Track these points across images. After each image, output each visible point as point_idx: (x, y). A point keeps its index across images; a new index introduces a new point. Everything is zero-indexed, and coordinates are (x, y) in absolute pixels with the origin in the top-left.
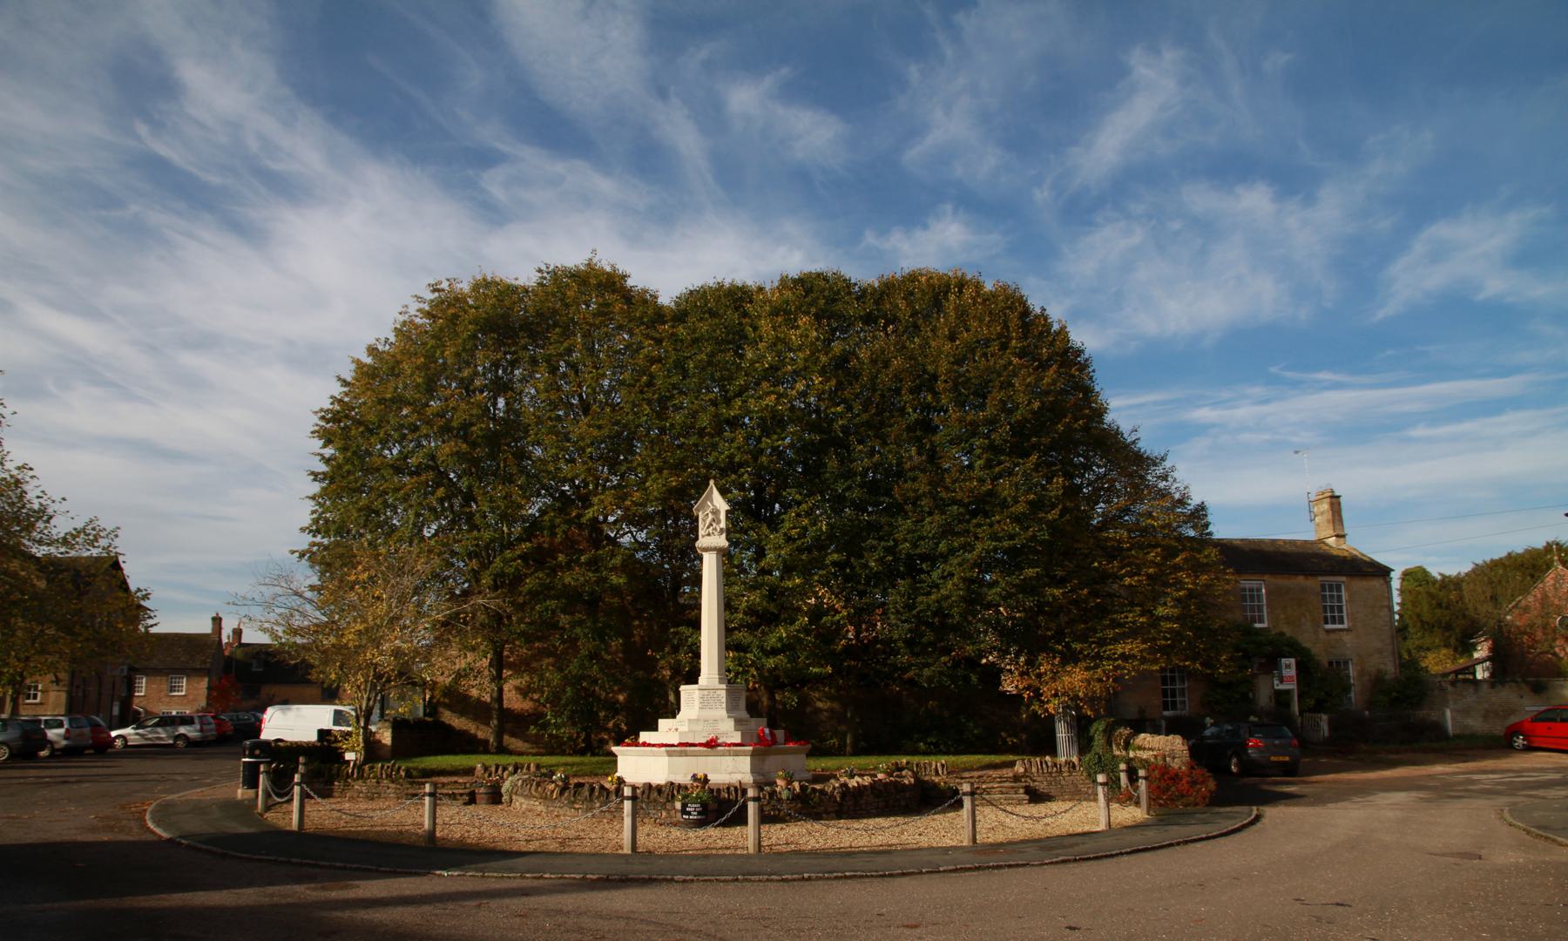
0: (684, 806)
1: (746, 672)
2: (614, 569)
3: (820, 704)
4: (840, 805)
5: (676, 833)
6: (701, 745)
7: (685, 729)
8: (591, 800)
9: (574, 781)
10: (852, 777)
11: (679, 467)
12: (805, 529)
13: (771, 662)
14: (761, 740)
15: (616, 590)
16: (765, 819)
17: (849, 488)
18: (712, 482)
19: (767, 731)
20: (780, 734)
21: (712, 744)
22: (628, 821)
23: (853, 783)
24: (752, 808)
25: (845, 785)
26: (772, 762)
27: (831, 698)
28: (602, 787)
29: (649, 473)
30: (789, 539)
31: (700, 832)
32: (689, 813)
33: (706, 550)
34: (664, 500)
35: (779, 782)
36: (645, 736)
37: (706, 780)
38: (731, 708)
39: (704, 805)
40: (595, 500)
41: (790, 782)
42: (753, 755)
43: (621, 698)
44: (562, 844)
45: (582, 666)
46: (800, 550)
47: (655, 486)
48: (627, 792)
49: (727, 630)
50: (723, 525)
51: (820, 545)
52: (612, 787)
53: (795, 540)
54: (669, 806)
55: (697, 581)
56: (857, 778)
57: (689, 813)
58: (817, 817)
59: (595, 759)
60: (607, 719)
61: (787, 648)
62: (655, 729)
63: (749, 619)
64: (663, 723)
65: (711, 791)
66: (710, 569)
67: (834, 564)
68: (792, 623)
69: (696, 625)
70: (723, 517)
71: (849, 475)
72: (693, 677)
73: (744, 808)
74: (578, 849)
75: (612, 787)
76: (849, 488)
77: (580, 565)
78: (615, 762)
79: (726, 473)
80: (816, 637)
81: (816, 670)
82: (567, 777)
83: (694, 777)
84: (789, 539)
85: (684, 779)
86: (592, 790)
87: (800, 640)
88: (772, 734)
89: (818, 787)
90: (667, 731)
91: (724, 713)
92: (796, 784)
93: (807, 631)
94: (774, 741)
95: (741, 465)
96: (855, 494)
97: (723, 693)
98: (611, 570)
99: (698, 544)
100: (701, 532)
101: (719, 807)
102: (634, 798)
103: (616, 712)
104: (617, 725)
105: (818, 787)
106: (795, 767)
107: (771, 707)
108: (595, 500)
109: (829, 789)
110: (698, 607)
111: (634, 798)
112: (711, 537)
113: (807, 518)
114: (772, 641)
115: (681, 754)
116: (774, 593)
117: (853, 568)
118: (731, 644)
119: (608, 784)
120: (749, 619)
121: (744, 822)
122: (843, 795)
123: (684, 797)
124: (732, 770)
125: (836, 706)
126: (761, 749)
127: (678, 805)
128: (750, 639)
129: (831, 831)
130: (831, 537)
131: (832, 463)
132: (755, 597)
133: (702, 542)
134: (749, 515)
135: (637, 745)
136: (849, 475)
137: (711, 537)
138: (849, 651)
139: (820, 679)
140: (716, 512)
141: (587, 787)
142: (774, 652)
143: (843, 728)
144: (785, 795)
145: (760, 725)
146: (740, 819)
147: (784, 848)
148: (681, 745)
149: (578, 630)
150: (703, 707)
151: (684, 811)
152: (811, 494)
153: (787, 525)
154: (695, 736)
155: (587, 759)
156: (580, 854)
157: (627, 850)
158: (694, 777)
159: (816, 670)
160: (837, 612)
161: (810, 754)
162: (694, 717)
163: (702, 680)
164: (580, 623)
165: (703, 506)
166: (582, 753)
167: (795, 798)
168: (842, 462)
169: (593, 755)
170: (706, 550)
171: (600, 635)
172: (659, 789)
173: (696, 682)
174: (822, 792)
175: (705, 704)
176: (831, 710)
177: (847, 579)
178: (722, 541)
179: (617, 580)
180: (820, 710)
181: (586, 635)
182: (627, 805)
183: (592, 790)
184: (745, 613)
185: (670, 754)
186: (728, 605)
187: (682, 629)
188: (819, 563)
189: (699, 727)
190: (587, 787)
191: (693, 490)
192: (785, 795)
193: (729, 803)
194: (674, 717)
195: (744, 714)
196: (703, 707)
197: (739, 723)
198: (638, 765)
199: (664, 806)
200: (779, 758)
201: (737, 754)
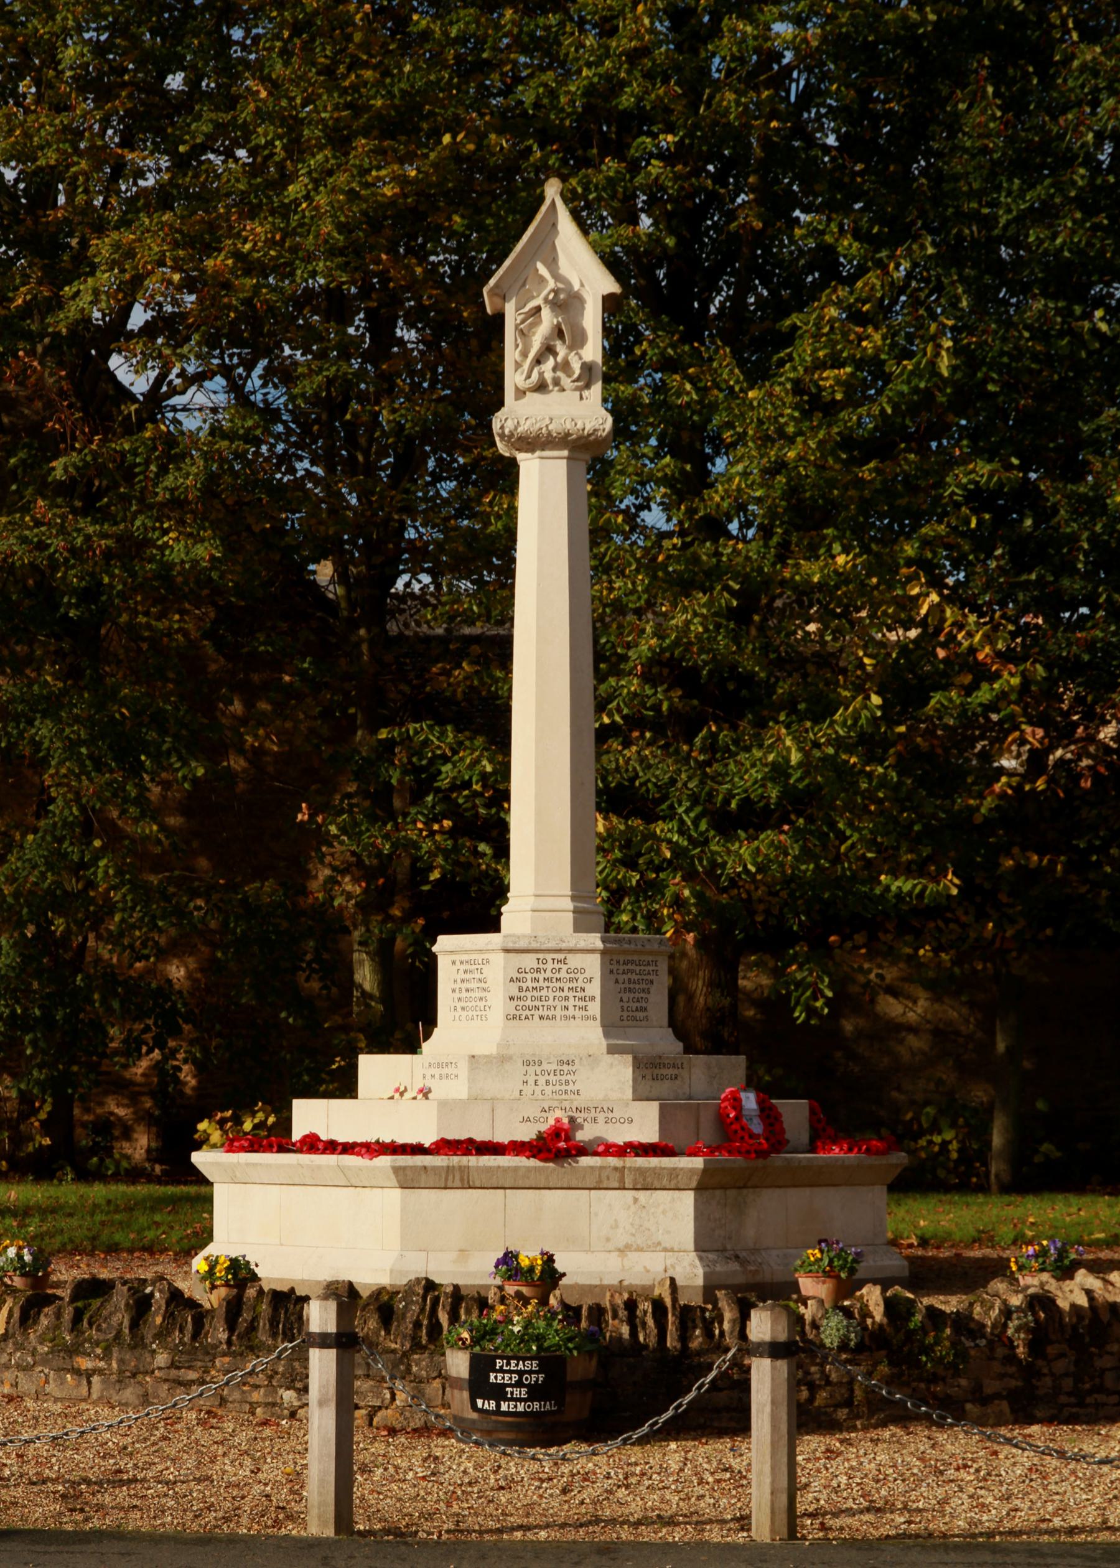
0: (481, 1366)
1: (650, 889)
2: (177, 503)
3: (892, 1008)
4: (1028, 1371)
5: (461, 1460)
6: (517, 1148)
7: (457, 1089)
8: (138, 1343)
9: (66, 1274)
10: (1065, 1272)
11: (402, 127)
12: (874, 366)
13: (742, 855)
14: (729, 1133)
15: (169, 588)
16: (806, 1417)
17: (1045, 214)
18: (552, 189)
19: (750, 1101)
20: (794, 1113)
21: (556, 1146)
22: (321, 1422)
23: (1072, 1293)
24: (765, 1380)
25: (1042, 1302)
26: (772, 1212)
27: (939, 987)
28: (176, 1297)
29: (297, 149)
30: (814, 405)
31: (544, 1459)
32: (498, 1393)
33: (532, 443)
34: (350, 254)
35: (808, 1285)
36: (309, 1115)
37: (548, 1275)
38: (619, 1020)
39: (552, 1364)
40: (102, 248)
41: (846, 1286)
42: (706, 1186)
43: (177, 972)
44: (71, 1498)
45: (56, 860)
46: (857, 448)
47: (319, 197)
48: (320, 1317)
49: (605, 730)
50: (593, 350)
51: (922, 419)
52: (212, 1299)
53: (830, 409)
54: (420, 1365)
55: (496, 553)
56: (1083, 1278)
57: (498, 1393)
58: (950, 1410)
59: (98, 1191)
60: (132, 1049)
61: (800, 803)
62: (345, 1085)
63: (665, 698)
64: (375, 1070)
65: (572, 1313)
66: (543, 508)
67: (977, 497)
68: (822, 710)
69: (489, 720)
70: (592, 319)
71: (1038, 158)
72: (477, 904)
73: (737, 1385)
74: (135, 1522)
75: (212, 1299)
76: (1045, 214)
77: (46, 488)
78: (209, 1200)
79: (590, 139)
80: (902, 767)
81: (903, 885)
82: (42, 1260)
83: (508, 1262)
84: (814, 405)
85: (477, 1270)
86: (141, 1306)
87: (844, 775)
88: (768, 1114)
89: (950, 1304)
90: (390, 1094)
91: (592, 1035)
92: (873, 1297)
93: (870, 744)
94: (776, 1139)
95: (638, 121)
96: (1066, 235)
97: (593, 965)
98: (163, 510)
99: (505, 421)
100: (513, 379)
101: (611, 1375)
102: (344, 1341)
103: (169, 1028)
104: (164, 1074)
105: (950, 1304)
106: (852, 1225)
107: (751, 1003)
108: (102, 248)
109: (987, 1315)
110: (499, 651)
111: (344, 1341)
112: (550, 400)
113: (873, 327)
114: (746, 776)
115: (447, 1181)
116: (752, 605)
117: (1045, 514)
118: (614, 798)
119: (193, 1277)
120: (665, 698)
121: (735, 1422)
122: (1038, 1338)
123: (482, 1335)
124: (633, 1240)
125: (952, 1012)
126: (735, 1165)
127: (458, 1363)
128: (664, 770)
129: (1014, 1463)
130: (966, 393)
131: (980, 115)
132: (689, 617)
133: (518, 413)
134: (657, 298)
135: (285, 1147)
136: (1038, 158)
137: (550, 400)
138: (1021, 816)
139: (913, 918)
140: (567, 303)
141: (120, 1298)
142: (750, 818)
143: (980, 1094)
144: (832, 1331)
145: (720, 1079)
146: (726, 1416)
147: (863, 1525)
148: (444, 1146)
149: (43, 730)
150: (522, 1013)
151: (479, 1385)
152: (898, 234)
153: (805, 350)
154: (491, 1118)
155: (68, 1191)
156: (155, 1539)
157: (318, 1523)
158: (508, 1262)
159: (903, 885)
160: (983, 674)
161: (904, 1185)
162: (489, 1047)
163: (515, 915)
164: (51, 705)
165: (522, 280)
166: (41, 1168)
167: (869, 1343)
168: (1015, 105)
169: (85, 1176)
170: (532, 443)
171: (122, 748)
172: (384, 1304)
173: (492, 925)
174: (963, 1323)
175: (525, 1004)
176: (941, 1033)
177: (1023, 555)
178: (590, 413)
179: (186, 549)
180: (897, 1028)
181: (72, 746)
182: (322, 1365)
183: (141, 1306)
184: (647, 678)
185: (407, 1181)
186: (601, 653)
187: (419, 729)
188: (909, 503)
189: (506, 1084)
190: (120, 1298)
191: (500, 217)
192: (832, 1331)
193: (679, 1369)
194: (412, 1047)
195: (669, 1045)
196: (522, 1013)
197: (649, 1072)
198: (291, 1215)
199: (400, 1367)
200: (797, 1198)
201: (646, 1183)
